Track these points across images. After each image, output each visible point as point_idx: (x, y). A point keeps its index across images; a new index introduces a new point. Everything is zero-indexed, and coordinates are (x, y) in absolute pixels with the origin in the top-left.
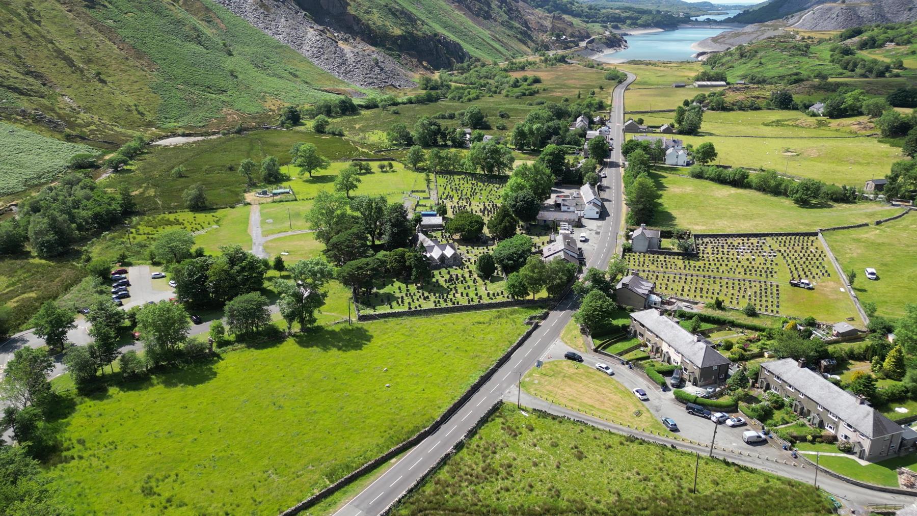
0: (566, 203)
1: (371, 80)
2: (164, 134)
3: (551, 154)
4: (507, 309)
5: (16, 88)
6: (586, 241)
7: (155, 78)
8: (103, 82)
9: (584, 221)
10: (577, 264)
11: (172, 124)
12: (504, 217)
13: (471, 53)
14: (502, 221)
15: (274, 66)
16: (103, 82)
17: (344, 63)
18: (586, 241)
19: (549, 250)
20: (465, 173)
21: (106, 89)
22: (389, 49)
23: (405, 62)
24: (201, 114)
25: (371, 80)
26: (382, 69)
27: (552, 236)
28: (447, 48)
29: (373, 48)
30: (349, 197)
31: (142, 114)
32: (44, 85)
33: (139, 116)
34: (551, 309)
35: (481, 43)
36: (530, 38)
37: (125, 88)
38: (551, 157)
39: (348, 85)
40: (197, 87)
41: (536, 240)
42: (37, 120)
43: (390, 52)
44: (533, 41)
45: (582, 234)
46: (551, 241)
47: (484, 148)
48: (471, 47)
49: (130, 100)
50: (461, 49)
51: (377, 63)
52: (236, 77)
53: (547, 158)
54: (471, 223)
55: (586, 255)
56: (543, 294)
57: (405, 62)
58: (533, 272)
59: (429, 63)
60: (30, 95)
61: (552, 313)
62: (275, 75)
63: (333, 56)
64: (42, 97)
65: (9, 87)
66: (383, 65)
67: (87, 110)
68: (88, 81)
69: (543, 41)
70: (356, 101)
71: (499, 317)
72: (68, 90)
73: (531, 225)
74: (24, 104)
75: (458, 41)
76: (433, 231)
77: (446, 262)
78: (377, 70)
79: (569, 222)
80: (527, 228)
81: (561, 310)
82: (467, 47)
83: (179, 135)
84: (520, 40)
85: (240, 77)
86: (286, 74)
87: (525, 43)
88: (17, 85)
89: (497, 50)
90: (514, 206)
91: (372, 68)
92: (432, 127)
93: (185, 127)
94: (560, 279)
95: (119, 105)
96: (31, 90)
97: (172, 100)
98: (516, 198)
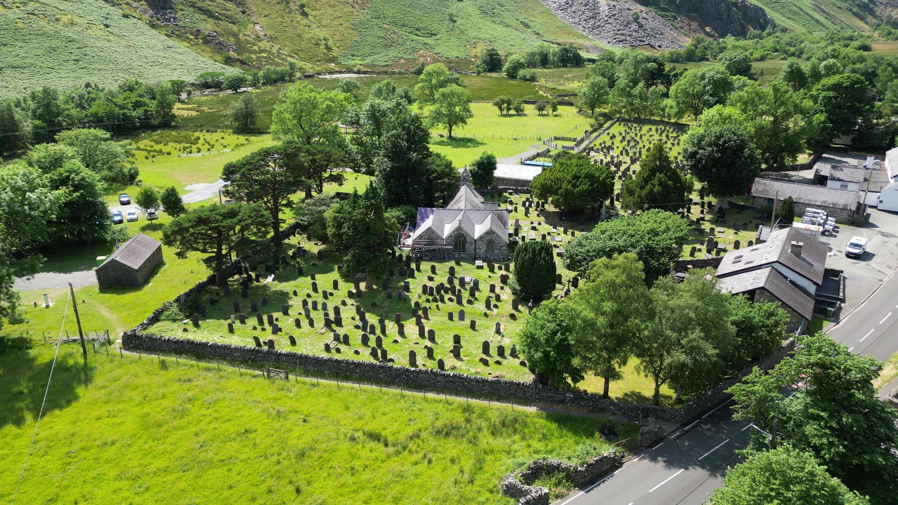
0: (838, 174)
1: (623, 37)
2: (337, 69)
3: (836, 87)
4: (498, 409)
5: (208, 10)
6: (863, 256)
7: (362, 15)
8: (305, 14)
9: (875, 216)
10: (807, 308)
11: (351, 63)
12: (653, 172)
13: (778, 22)
14: (646, 181)
15: (505, 14)
16: (305, 14)
17: (593, 17)
18: (863, 256)
19: (738, 260)
20: (667, 124)
21: (305, 21)
22: (663, 9)
23: (681, 24)
24: (393, 53)
25: (623, 37)
26: (641, 26)
27: (765, 230)
28: (745, 14)
29: (643, 8)
30: (450, 137)
31: (329, 49)
32: (244, 13)
33: (325, 51)
34: (635, 449)
35: (795, 13)
36: (872, 12)
37: (324, 23)
38: (831, 94)
39: (591, 40)
40: (404, 28)
41: (725, 236)
42: (207, 40)
43: (663, 13)
44: (875, 17)
45: (854, 240)
46: (759, 241)
47: (703, 78)
48: (780, 17)
49: (321, 33)
50: (764, 14)
51: (636, 20)
52: (455, 21)
53: (823, 94)
54: (576, 177)
55: (850, 290)
56: (634, 380)
57: (681, 24)
58: (598, 310)
59: (714, 28)
60: (220, 19)
61: (635, 467)
62: (502, 23)
63: (583, 9)
64: (234, 23)
65: (200, 9)
66: (644, 22)
67: (272, 39)
68: (290, 12)
69: (890, 17)
70: (584, 55)
71: (446, 432)
72: (263, 19)
73: (733, 205)
74: (208, 26)
75: (760, 5)
76: (517, 192)
77: (470, 248)
78: (634, 26)
79: (831, 210)
80: (721, 209)
81: (672, 463)
82: (771, 13)
83: (354, 73)
84: (856, 15)
85: (459, 21)
86: (515, 23)
87: (862, 18)
88: (210, 8)
89: (817, 21)
90: (693, 155)
91: (629, 23)
92: (649, 65)
93: (366, 66)
94: (692, 350)
95: (309, 38)
96: (224, 15)
97: (369, 39)
98: (701, 139)
